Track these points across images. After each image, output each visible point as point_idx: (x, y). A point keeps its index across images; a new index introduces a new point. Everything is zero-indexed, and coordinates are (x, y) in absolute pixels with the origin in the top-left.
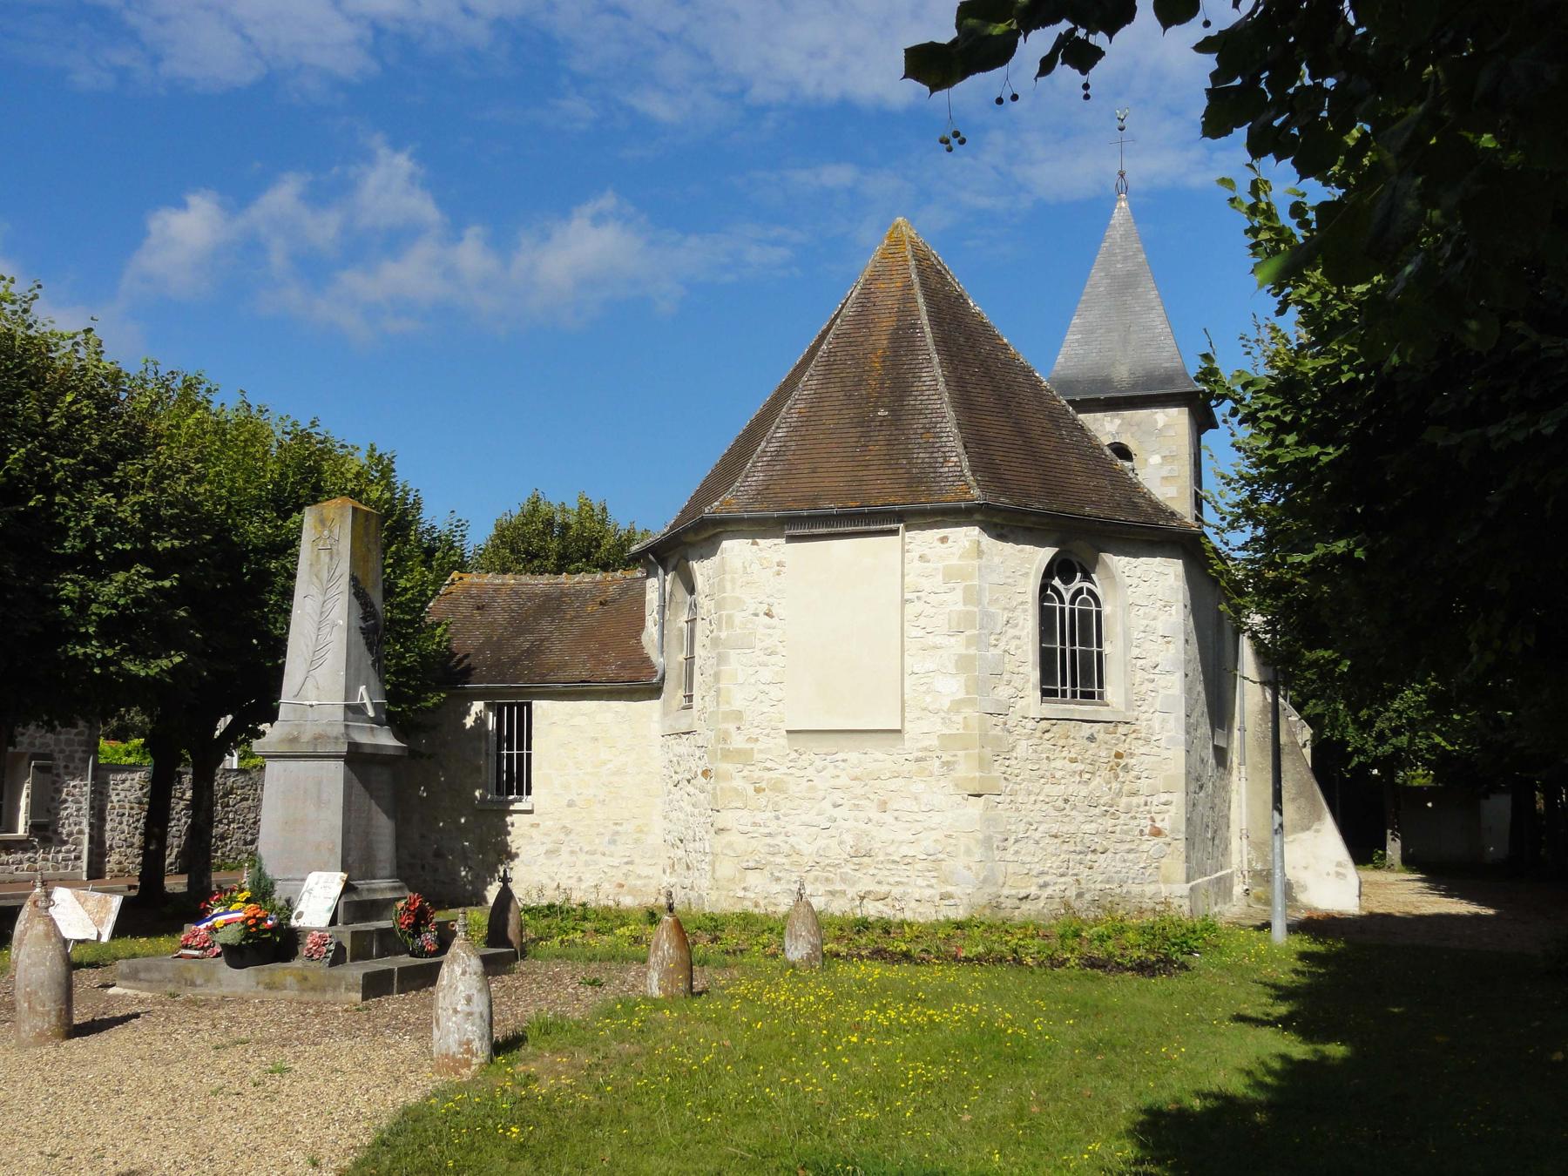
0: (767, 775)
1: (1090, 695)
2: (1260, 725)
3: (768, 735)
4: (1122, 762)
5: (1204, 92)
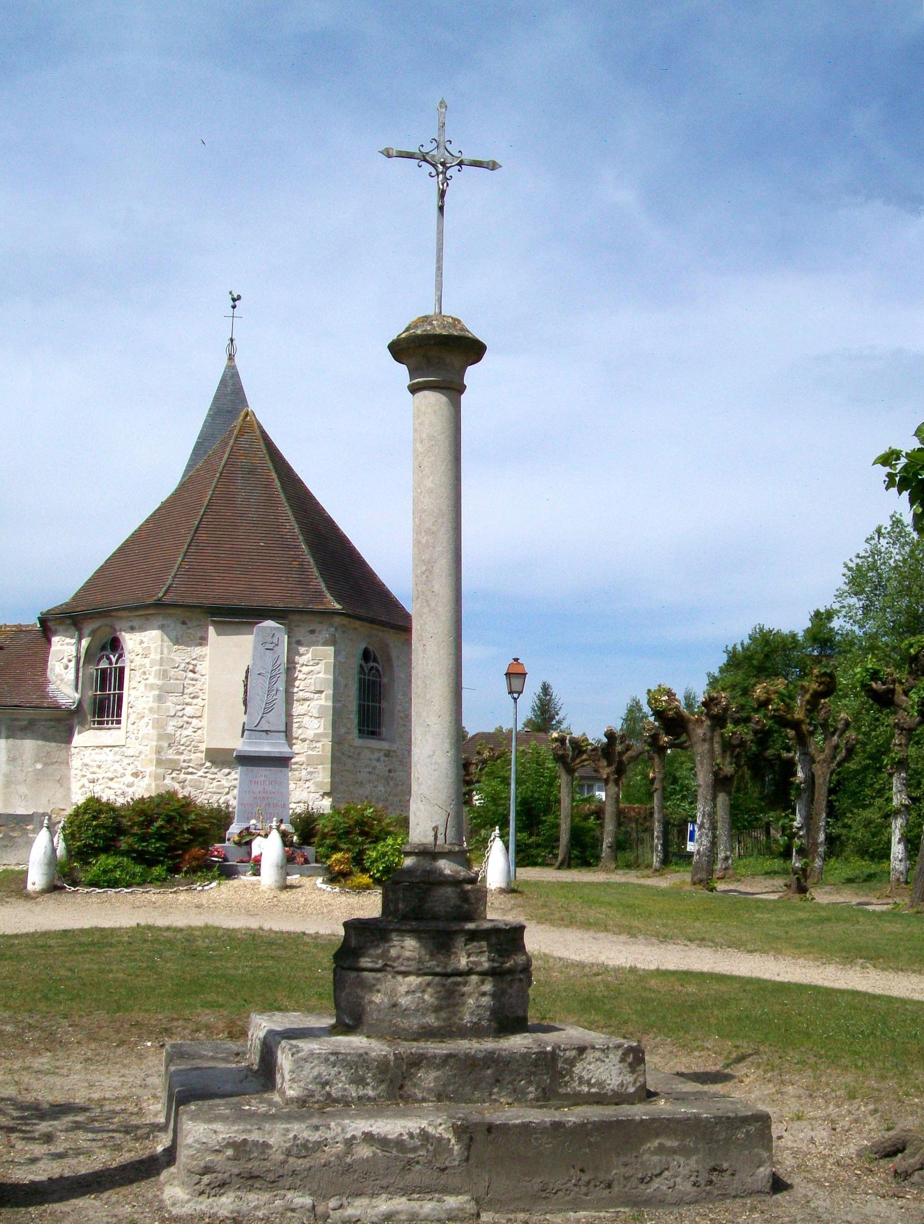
0: (189, 777)
1: (373, 733)
2: (534, 710)
3: (190, 751)
4: (392, 774)
5: (498, 726)
